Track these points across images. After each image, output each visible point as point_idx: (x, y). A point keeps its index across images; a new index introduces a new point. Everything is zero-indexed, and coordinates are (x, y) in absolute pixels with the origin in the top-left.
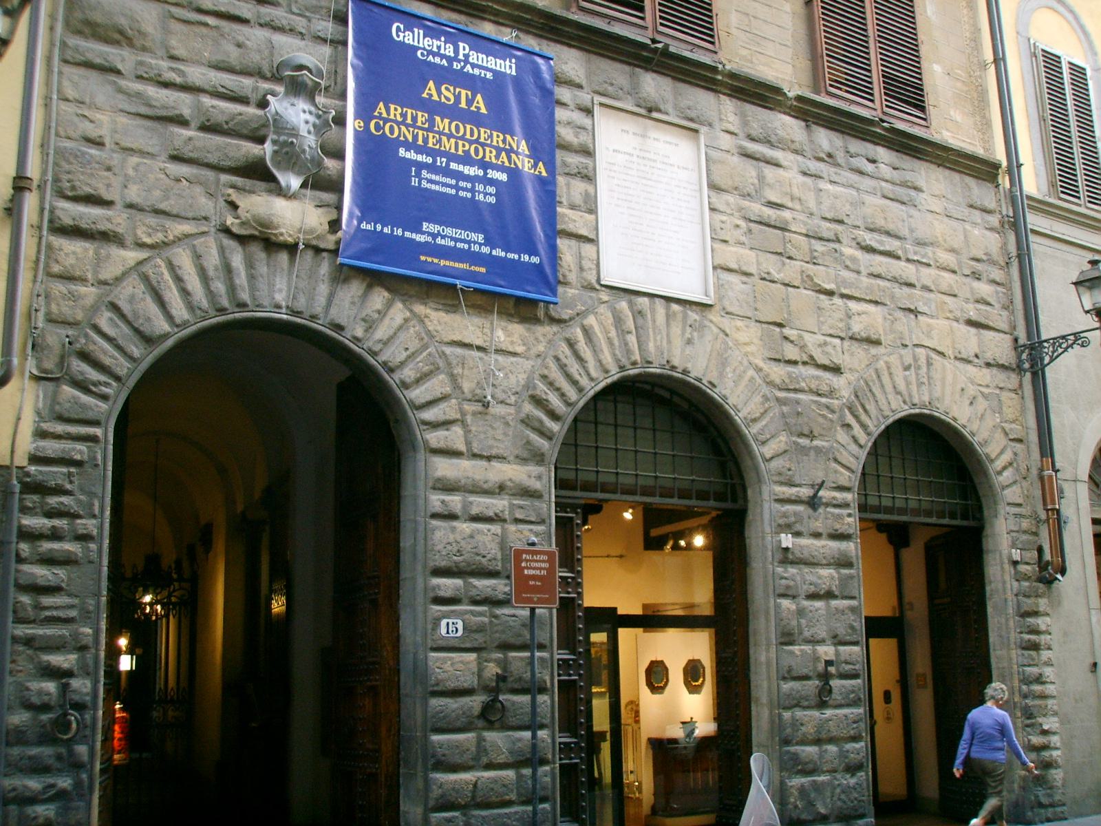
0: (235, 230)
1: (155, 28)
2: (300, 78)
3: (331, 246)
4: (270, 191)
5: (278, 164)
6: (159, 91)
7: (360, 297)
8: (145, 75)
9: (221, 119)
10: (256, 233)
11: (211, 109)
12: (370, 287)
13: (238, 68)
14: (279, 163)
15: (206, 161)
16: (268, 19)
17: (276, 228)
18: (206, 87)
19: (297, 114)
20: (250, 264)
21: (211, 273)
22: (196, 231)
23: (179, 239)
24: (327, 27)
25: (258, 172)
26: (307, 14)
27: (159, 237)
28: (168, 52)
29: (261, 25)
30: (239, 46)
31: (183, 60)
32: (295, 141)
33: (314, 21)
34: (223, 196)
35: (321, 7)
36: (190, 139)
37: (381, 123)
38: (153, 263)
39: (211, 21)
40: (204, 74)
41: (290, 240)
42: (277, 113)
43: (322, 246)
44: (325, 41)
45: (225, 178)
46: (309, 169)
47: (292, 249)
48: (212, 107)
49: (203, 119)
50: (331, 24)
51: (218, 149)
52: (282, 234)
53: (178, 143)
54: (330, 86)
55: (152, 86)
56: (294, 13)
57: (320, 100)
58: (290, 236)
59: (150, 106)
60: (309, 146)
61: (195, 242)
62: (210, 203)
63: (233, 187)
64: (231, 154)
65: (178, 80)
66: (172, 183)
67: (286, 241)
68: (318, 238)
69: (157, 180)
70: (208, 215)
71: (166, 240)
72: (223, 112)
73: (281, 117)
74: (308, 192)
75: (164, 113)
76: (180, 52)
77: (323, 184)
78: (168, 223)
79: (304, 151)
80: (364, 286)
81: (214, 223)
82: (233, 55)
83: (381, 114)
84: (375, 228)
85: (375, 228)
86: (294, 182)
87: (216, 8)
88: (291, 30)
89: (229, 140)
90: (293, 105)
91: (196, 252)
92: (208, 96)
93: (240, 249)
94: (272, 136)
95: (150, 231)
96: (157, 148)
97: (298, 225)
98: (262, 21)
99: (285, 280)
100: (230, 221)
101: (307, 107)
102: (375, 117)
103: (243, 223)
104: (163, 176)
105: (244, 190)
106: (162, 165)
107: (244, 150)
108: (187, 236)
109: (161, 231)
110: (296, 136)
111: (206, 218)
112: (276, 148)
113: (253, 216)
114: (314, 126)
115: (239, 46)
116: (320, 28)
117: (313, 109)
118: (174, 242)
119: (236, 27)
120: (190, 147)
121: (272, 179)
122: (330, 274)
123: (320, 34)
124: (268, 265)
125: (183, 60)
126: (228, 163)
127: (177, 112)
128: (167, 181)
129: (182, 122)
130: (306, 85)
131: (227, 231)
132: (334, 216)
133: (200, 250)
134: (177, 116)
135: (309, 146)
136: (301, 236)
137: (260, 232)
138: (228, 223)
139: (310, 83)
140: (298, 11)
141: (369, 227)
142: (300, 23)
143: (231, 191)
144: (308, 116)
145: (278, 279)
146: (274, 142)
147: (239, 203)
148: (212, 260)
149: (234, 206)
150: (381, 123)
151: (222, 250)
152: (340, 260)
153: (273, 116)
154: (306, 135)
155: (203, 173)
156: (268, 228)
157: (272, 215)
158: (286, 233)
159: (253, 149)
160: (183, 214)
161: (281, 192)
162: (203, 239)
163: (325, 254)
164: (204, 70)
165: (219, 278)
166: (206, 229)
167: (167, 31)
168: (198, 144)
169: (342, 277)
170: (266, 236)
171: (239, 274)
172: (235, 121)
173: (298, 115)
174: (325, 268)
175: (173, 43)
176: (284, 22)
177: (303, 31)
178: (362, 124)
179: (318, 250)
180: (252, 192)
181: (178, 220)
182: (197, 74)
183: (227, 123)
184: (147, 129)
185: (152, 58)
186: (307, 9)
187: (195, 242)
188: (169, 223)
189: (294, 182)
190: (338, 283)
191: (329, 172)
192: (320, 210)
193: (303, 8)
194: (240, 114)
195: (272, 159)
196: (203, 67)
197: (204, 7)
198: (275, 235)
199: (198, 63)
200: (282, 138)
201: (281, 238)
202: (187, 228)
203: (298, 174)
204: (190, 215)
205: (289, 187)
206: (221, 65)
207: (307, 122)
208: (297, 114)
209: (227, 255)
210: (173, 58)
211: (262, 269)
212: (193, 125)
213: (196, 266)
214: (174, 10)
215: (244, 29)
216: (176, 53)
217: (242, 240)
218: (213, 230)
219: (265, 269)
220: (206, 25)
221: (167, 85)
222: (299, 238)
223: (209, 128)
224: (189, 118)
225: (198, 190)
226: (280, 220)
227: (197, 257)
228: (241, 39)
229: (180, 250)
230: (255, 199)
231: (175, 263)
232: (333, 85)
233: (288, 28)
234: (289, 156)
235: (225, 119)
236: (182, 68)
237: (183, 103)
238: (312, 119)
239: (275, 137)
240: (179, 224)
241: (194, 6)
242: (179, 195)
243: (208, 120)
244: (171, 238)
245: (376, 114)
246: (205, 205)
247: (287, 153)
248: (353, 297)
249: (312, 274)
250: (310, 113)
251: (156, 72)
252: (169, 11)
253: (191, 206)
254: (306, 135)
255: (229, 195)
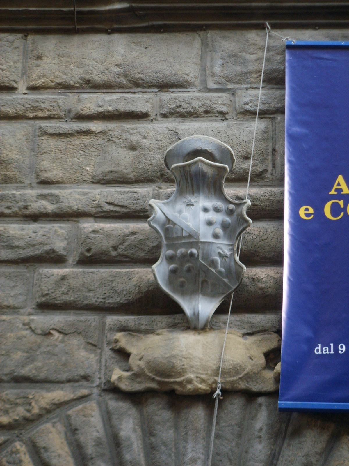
0: (124, 386)
1: (21, 151)
2: (193, 168)
3: (270, 387)
4: (173, 327)
5: (182, 290)
6: (25, 226)
7: (320, 454)
8: (7, 211)
9: (106, 244)
10: (154, 385)
11: (92, 235)
12: (335, 439)
13: (131, 176)
14: (182, 285)
15: (86, 302)
16: (173, 106)
17: (180, 374)
18: (88, 209)
19: (197, 216)
20: (148, 431)
21: (90, 450)
22: (72, 396)
23: (47, 412)
24: (258, 96)
25: (156, 305)
26: (230, 86)
27: (21, 412)
28: (38, 176)
29: (164, 116)
30: (133, 148)
31: (58, 182)
32: (195, 251)
33: (239, 92)
34: (109, 343)
35: (250, 73)
36: (64, 278)
37: (341, 203)
38: (9, 449)
39: (95, 126)
40: (85, 194)
41: (203, 386)
42: (168, 220)
43: (255, 387)
44: (253, 113)
45: (111, 319)
46: (225, 284)
47: (205, 398)
48: (94, 232)
49: (82, 249)
50: (260, 92)
51: (103, 283)
52: (190, 381)
53: (46, 287)
54: (265, 171)
55: (16, 222)
56: (210, 90)
57: (229, 191)
58: (203, 381)
59: (12, 247)
60: (220, 255)
61: (70, 412)
62: (92, 356)
63: (123, 329)
64: (120, 288)
65: (50, 207)
66: (39, 339)
67: (196, 390)
68: (248, 377)
69: (19, 338)
70: (89, 372)
71: (28, 415)
72: (108, 236)
73: (174, 224)
74: (229, 317)
75: (29, 252)
76: (54, 172)
77: (246, 302)
78: (32, 392)
79: (213, 263)
80: (325, 437)
81: (97, 382)
82: (123, 160)
83: (339, 191)
84: (336, 350)
85: (336, 350)
86: (204, 307)
87: (101, 110)
88: (207, 112)
89: (115, 270)
90: (190, 205)
91: (70, 425)
92: (92, 219)
93: (133, 411)
94: (165, 252)
95: (8, 406)
96: (21, 298)
97: (212, 364)
98: (165, 110)
99: (200, 446)
100: (117, 374)
101: (209, 204)
102: (333, 197)
103: (136, 376)
104: (27, 333)
105: (139, 331)
106: (26, 319)
107: (135, 280)
108: (60, 405)
109: (23, 404)
110: (196, 244)
111: (86, 378)
112: (172, 266)
113: (148, 362)
114: (225, 226)
115: (133, 148)
116: (247, 99)
117: (220, 204)
118: (40, 416)
119: (128, 126)
120: (64, 289)
121: (178, 310)
122: (271, 426)
123: (248, 107)
124: (176, 428)
125: (58, 182)
126: (116, 300)
127: (47, 248)
128: (33, 338)
129: (55, 259)
130: (204, 175)
131: (113, 390)
132: (273, 345)
133: (76, 421)
134: (47, 252)
135: (220, 255)
136: (219, 379)
137: (159, 383)
138: (114, 378)
139: (209, 171)
140: (215, 86)
141: (326, 350)
142: (220, 101)
143: (118, 335)
144: (212, 216)
145: (190, 446)
146: (170, 259)
147: (130, 349)
148: (93, 428)
149: (123, 354)
150: (341, 203)
151: (108, 417)
152: (282, 404)
153: (163, 226)
154: (211, 240)
155: (82, 318)
156: (170, 376)
157: (173, 356)
158: (196, 379)
159: (139, 275)
160: (53, 377)
161: (189, 325)
162: (81, 406)
163: (261, 400)
164: (85, 188)
165: (102, 456)
166: (85, 392)
167: (37, 152)
168: (73, 283)
169: (290, 429)
170: (167, 388)
171: (130, 446)
172: (126, 244)
173: (195, 216)
174: (262, 419)
175: (45, 164)
176: (196, 104)
177: (224, 109)
178: (311, 211)
179: (250, 396)
180: (150, 331)
181: (47, 385)
182: (73, 197)
183: (115, 248)
184: (9, 277)
185: (17, 188)
186: (229, 81)
187: (70, 412)
188: (33, 392)
189: (204, 307)
190: (284, 439)
191: (260, 285)
192: (251, 339)
193: (223, 80)
194: (133, 233)
195: (170, 282)
196: (86, 186)
197: (86, 112)
198: (180, 383)
199: (80, 182)
200: (181, 251)
201: (189, 386)
202: (58, 394)
203: (213, 295)
204: (64, 376)
205: (196, 315)
206: (108, 178)
207: (210, 223)
208: (197, 216)
209: (115, 422)
210: (45, 183)
211: (166, 434)
212: (71, 260)
213: (70, 444)
214: (45, 124)
215: (142, 126)
216: (49, 175)
217: (136, 398)
218: (96, 391)
219: (171, 433)
220: (88, 133)
221: (36, 217)
222: (215, 382)
223: (91, 259)
224: (64, 253)
225: (75, 341)
226: (185, 361)
227: (72, 431)
228: (134, 139)
229: (49, 425)
230: (153, 339)
231: (41, 443)
232: (270, 168)
233: (202, 110)
234: (193, 273)
235: (112, 243)
236: (56, 192)
237: (56, 236)
238: (218, 218)
239: (170, 252)
240: (49, 391)
241: (73, 114)
242: (48, 353)
243: (89, 250)
244: (36, 411)
245: (333, 192)
246: (85, 359)
247: (189, 270)
248: (307, 455)
249: (242, 431)
250: (217, 210)
251: (21, 204)
252: (40, 128)
253: (65, 365)
254: (211, 240)
255: (116, 341)
